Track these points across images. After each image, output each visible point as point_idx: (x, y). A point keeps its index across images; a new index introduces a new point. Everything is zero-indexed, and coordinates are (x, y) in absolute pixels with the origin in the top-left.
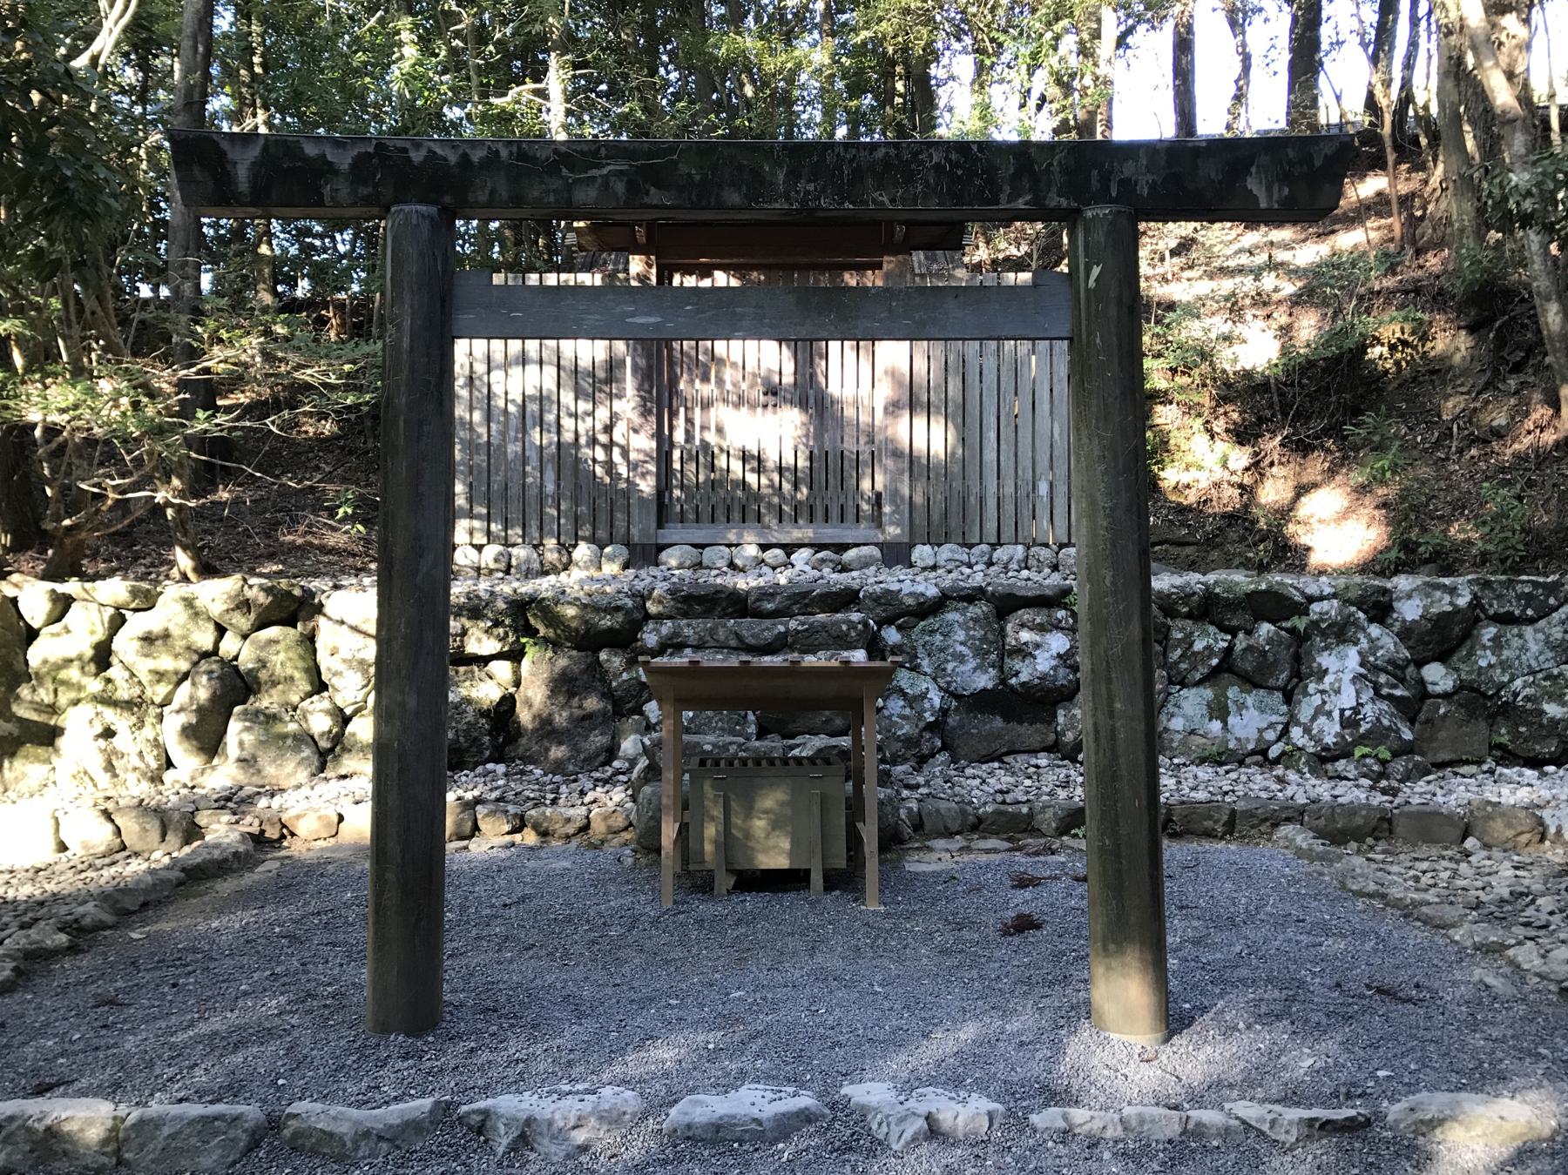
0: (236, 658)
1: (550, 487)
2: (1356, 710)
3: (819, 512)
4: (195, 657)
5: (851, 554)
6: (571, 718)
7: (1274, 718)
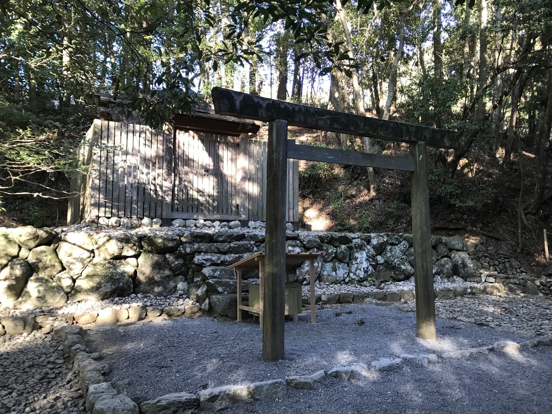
0: (26, 258)
1: (135, 198)
2: (367, 268)
4: (10, 258)
5: (232, 223)
6: (161, 277)
7: (346, 271)
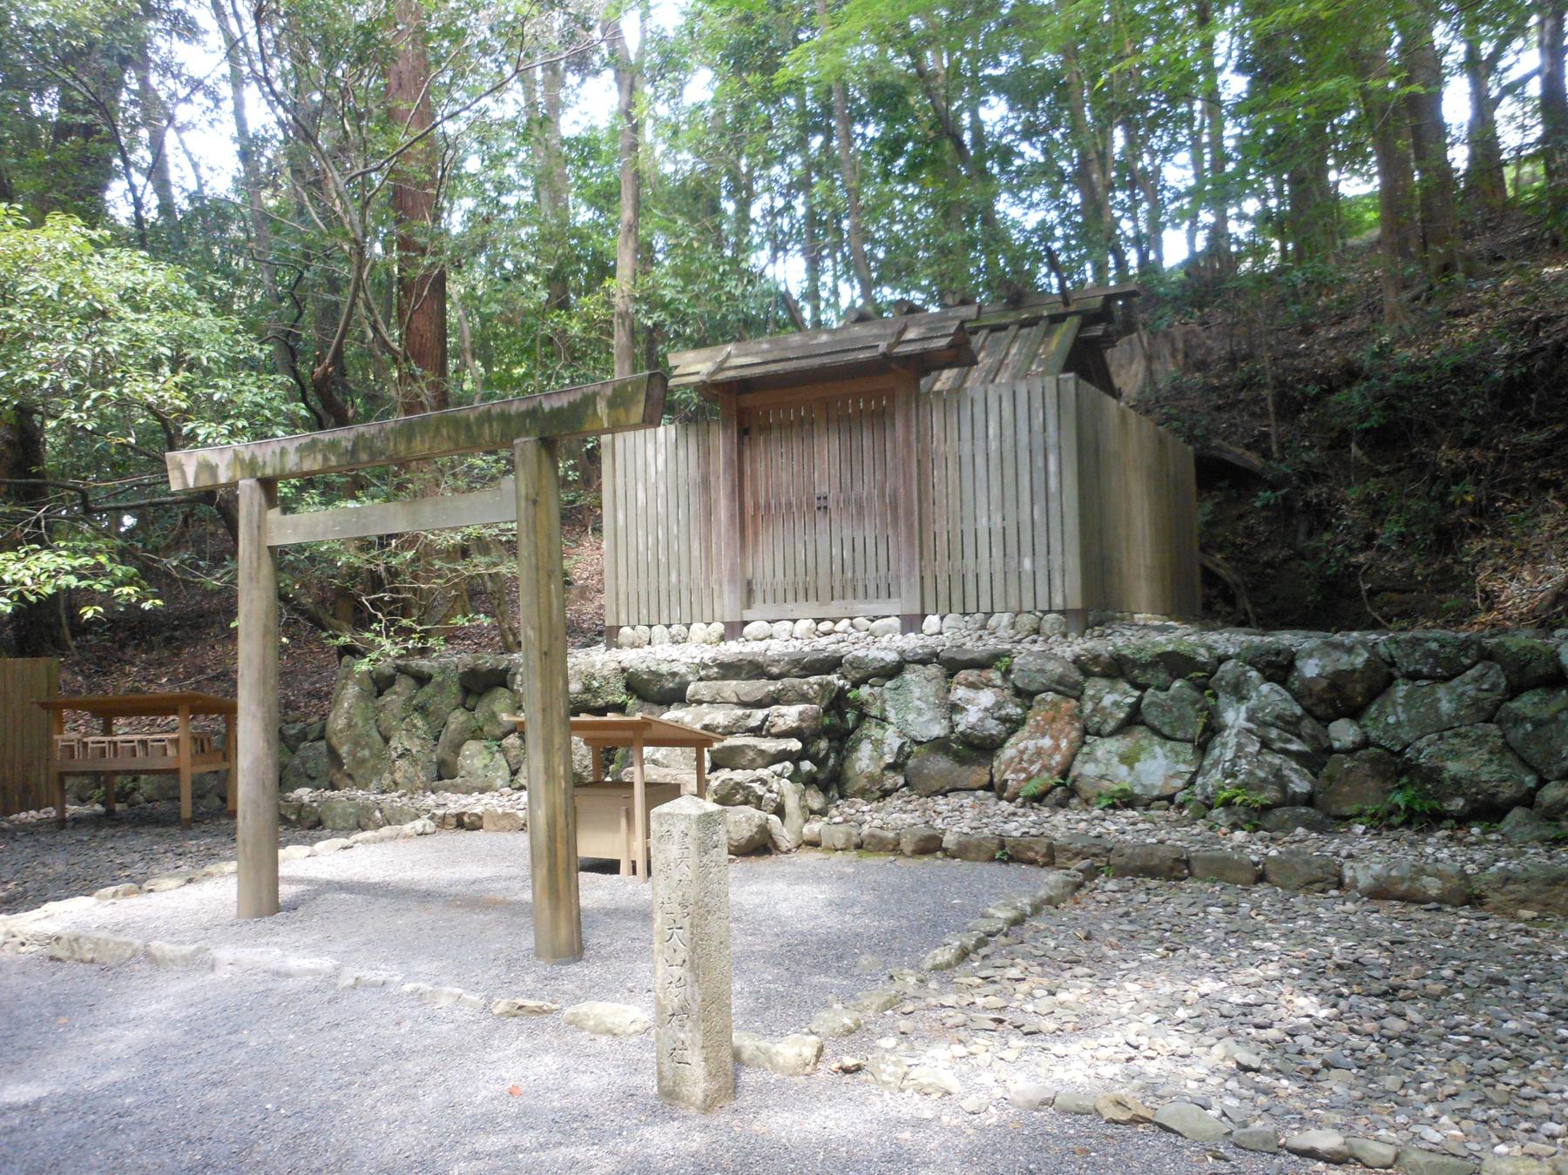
3: (860, 590)
